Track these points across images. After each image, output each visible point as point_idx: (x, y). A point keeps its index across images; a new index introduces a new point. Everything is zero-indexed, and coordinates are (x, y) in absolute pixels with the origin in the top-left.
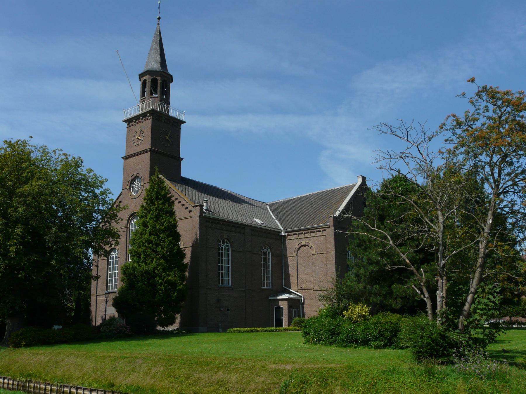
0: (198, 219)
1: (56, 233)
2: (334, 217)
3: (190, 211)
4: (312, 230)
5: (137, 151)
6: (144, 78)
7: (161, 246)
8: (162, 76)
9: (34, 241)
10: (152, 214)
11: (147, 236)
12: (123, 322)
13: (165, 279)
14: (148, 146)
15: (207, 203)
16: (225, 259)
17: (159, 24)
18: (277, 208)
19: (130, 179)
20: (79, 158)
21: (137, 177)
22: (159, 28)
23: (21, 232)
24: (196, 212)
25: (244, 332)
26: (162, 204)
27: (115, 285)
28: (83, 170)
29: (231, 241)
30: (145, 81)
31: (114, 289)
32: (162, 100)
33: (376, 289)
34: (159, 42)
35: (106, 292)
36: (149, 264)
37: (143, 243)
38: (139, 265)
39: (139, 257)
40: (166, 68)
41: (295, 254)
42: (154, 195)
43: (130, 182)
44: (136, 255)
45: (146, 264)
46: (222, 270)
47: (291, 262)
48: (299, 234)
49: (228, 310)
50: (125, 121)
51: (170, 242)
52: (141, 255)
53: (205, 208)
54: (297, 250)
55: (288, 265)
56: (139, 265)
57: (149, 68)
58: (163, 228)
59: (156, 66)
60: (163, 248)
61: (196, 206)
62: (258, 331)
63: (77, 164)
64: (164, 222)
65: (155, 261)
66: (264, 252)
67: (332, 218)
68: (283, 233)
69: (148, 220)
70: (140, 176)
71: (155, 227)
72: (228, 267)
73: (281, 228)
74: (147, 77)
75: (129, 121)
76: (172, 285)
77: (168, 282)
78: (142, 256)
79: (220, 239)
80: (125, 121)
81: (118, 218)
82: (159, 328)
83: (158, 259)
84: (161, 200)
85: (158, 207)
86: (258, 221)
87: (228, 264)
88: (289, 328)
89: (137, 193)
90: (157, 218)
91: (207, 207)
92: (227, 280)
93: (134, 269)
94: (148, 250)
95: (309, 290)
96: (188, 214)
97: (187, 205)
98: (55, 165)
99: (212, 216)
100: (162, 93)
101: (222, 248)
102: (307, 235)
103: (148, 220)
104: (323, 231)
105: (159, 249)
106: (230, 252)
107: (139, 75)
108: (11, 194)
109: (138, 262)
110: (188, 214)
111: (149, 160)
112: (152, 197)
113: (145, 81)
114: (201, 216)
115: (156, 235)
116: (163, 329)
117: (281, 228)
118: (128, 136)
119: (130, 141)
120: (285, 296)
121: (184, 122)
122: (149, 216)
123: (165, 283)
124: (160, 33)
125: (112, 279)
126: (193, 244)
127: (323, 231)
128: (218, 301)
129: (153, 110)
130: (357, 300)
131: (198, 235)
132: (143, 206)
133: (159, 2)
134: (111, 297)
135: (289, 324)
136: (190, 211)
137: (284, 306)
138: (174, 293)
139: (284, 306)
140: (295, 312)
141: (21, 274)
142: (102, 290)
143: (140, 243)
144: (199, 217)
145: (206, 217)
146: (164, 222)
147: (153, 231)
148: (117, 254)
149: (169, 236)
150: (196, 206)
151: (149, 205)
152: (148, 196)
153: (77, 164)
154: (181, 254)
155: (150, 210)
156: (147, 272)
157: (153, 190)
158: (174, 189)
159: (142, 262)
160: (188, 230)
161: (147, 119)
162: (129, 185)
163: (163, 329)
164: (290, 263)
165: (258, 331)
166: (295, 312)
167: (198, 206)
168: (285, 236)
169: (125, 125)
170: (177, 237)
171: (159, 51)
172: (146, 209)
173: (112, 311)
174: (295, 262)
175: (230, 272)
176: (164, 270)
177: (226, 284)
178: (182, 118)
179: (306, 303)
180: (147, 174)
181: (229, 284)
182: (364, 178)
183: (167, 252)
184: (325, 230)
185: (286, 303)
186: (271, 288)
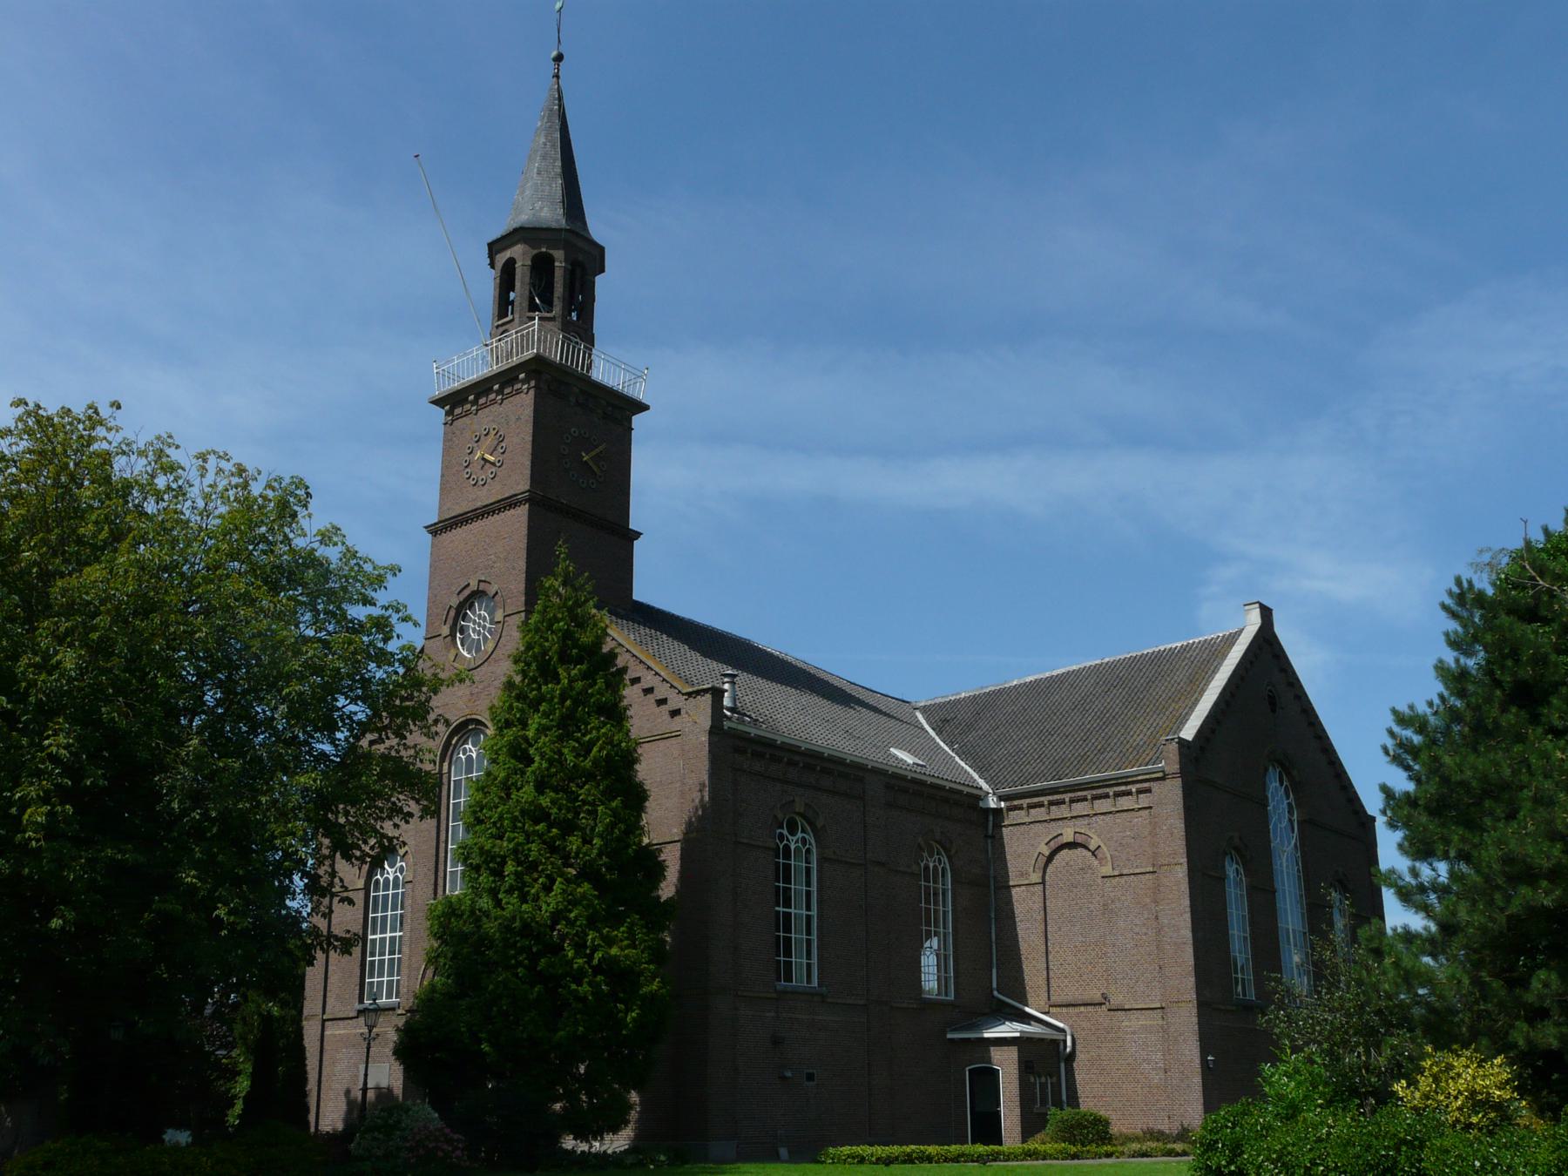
0: (705, 738)
1: (199, 757)
2: (1182, 742)
3: (675, 713)
4: (1098, 790)
5: (479, 504)
6: (507, 254)
7: (583, 829)
8: (568, 247)
9: (119, 785)
10: (546, 715)
11: (527, 793)
12: (427, 1114)
13: (598, 955)
14: (519, 481)
15: (733, 683)
16: (797, 887)
17: (557, 76)
18: (946, 717)
19: (455, 602)
20: (299, 483)
21: (478, 594)
22: (559, 90)
23: (67, 747)
24: (699, 715)
25: (879, 1160)
26: (584, 676)
27: (390, 983)
28: (306, 533)
29: (820, 823)
30: (511, 263)
31: (389, 996)
32: (567, 327)
33: (1546, 985)
34: (558, 135)
35: (358, 1006)
36: (536, 898)
37: (514, 820)
38: (498, 903)
39: (498, 873)
40: (585, 223)
41: (1035, 877)
42: (553, 643)
43: (452, 613)
44: (481, 863)
45: (523, 899)
46: (788, 929)
47: (1024, 903)
48: (1051, 803)
49: (810, 1077)
50: (438, 402)
51: (615, 813)
52: (504, 863)
53: (727, 702)
54: (1042, 860)
55: (1011, 916)
56: (498, 903)
57: (524, 218)
58: (588, 764)
59: (550, 214)
60: (587, 841)
61: (698, 693)
62: (930, 1159)
63: (289, 503)
64: (592, 743)
65: (557, 887)
66: (927, 868)
67: (1174, 746)
68: (992, 803)
69: (530, 734)
70: (492, 590)
71: (557, 761)
72: (809, 918)
73: (985, 786)
74: (518, 252)
75: (453, 402)
76: (621, 977)
77: (609, 968)
78: (510, 867)
79: (780, 816)
80: (438, 402)
81: (432, 717)
82: (569, 1143)
83: (568, 881)
84: (579, 661)
85: (571, 687)
86: (909, 759)
87: (808, 908)
88: (1032, 1145)
89: (478, 650)
90: (568, 725)
91: (734, 699)
92: (805, 969)
93: (476, 916)
94: (534, 846)
95: (1090, 1008)
96: (664, 723)
97: (662, 691)
98: (202, 501)
99: (753, 732)
100: (569, 302)
101: (787, 848)
102: (1080, 808)
103: (530, 734)
104: (1139, 792)
105: (574, 842)
106: (814, 865)
107: (490, 245)
108: (35, 606)
109: (493, 893)
110: (664, 723)
111: (525, 531)
112: (545, 653)
113: (511, 263)
114: (717, 730)
115: (566, 790)
116: (584, 1147)
117: (985, 786)
118: (447, 451)
119: (453, 473)
120: (1009, 1030)
121: (643, 408)
122: (535, 721)
123: (597, 970)
124: (561, 105)
125: (382, 962)
126: (690, 827)
127: (1139, 792)
128: (777, 1042)
129: (538, 359)
130: (1443, 1031)
131: (706, 795)
132: (509, 685)
133: (558, 5)
134: (389, 1031)
135: (1027, 1133)
136: (675, 713)
137: (1006, 1065)
138: (627, 1011)
139: (1006, 1065)
140: (1043, 1086)
141: (62, 917)
142: (342, 1000)
143: (501, 818)
144: (711, 733)
145: (734, 735)
146: (592, 743)
147: (551, 776)
148: (401, 870)
149: (609, 794)
150: (698, 693)
151: (534, 680)
152: (529, 647)
153: (289, 503)
154: (650, 863)
155: (541, 699)
156: (527, 929)
157: (550, 627)
158: (621, 637)
159: (510, 891)
160: (673, 781)
161: (519, 392)
162: (450, 621)
163: (584, 1147)
164: (1019, 909)
165: (930, 1159)
166: (1043, 1086)
167: (706, 691)
168: (998, 811)
169: (439, 413)
170: (636, 797)
171: (559, 163)
172: (521, 697)
173: (387, 1074)
174: (1039, 905)
175: (814, 937)
176: (592, 922)
177: (798, 981)
178: (639, 393)
179: (1081, 1057)
180: (515, 585)
181: (809, 981)
182: (1266, 613)
183: (600, 855)
184: (1148, 791)
185: (1012, 1053)
186: (952, 997)
